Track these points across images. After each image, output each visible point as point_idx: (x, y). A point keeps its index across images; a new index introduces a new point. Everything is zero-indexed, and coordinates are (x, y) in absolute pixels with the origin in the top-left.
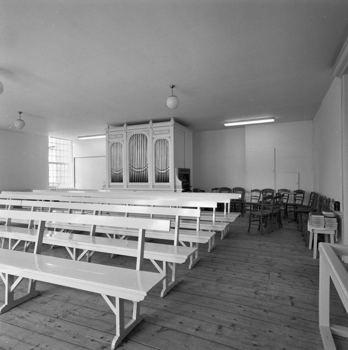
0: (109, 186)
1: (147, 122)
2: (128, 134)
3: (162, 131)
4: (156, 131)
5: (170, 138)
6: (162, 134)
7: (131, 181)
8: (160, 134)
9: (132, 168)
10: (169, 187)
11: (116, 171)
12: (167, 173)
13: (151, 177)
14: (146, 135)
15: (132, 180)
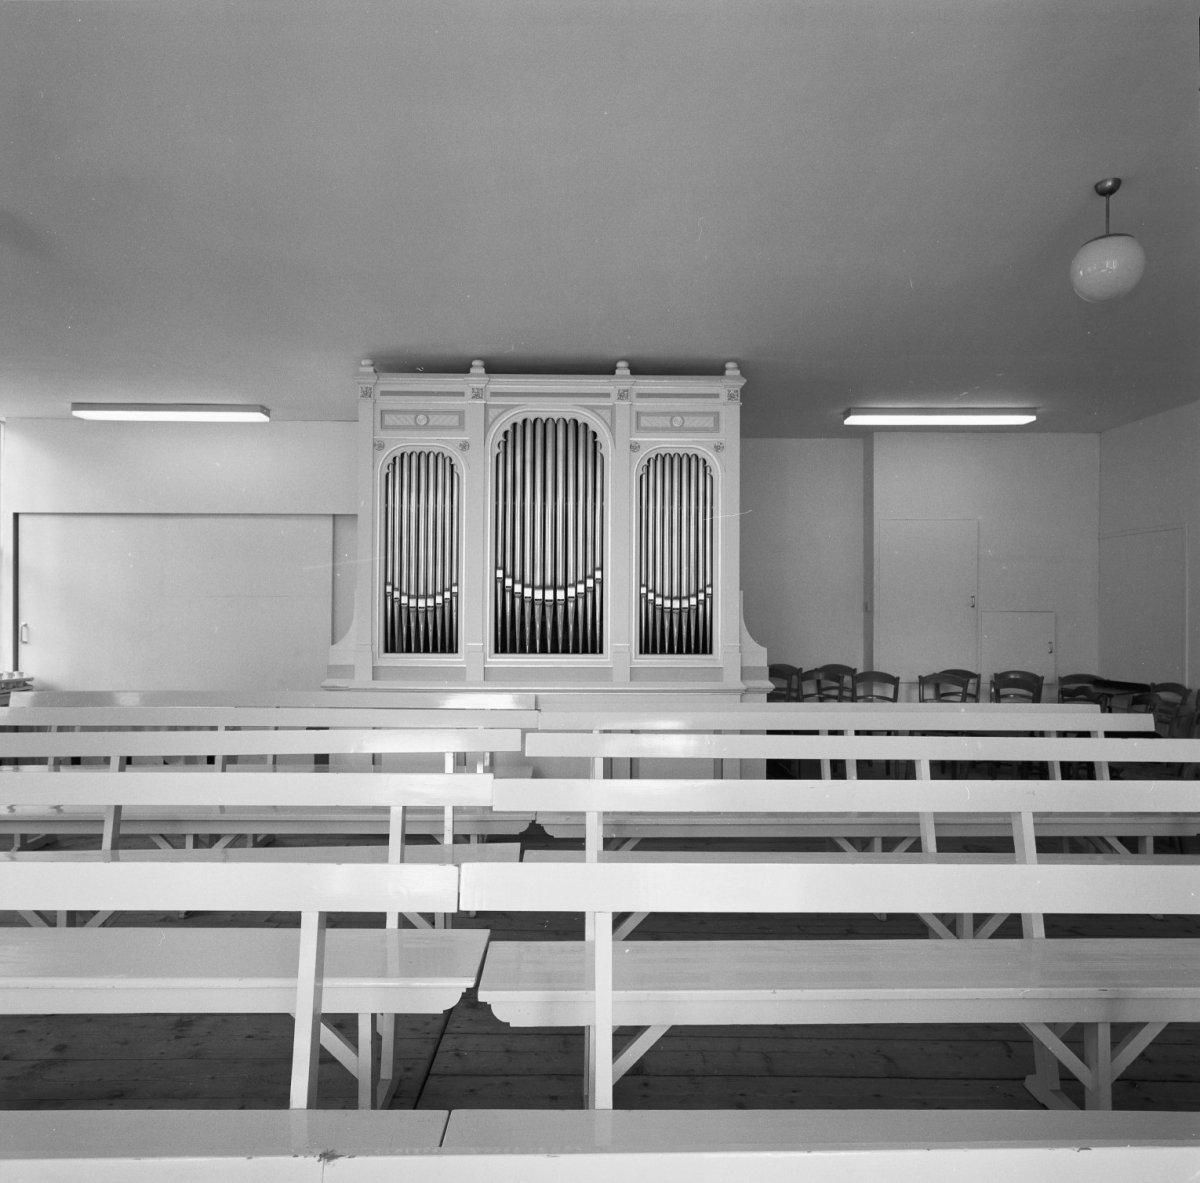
0: (376, 673)
1: (607, 369)
2: (491, 420)
3: (679, 414)
4: (648, 414)
5: (466, 453)
6: (426, 427)
7: (648, 646)
8: (417, 427)
9: (509, 582)
10: (716, 673)
11: (413, 592)
12: (697, 609)
13: (620, 625)
14: (596, 424)
15: (514, 634)
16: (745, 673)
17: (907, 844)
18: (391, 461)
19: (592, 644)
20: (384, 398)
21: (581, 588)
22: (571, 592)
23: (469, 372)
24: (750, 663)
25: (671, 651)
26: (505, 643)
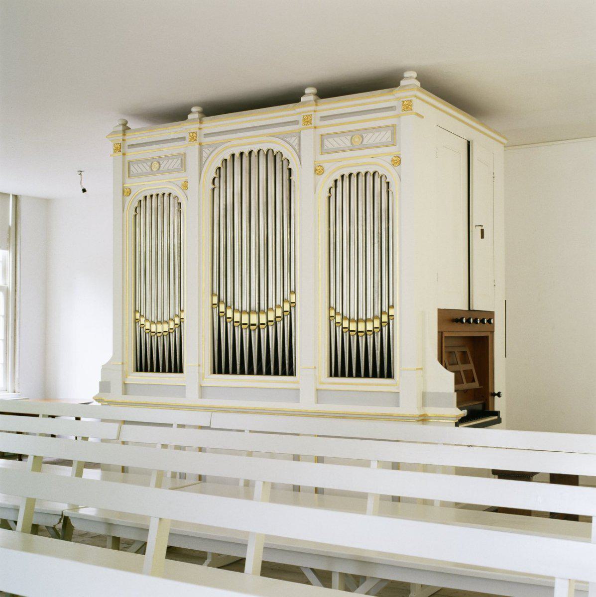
8: (151, 173)
12: (381, 330)
13: (312, 350)
16: (425, 399)
17: (136, 546)
18: (332, 184)
19: (285, 366)
20: (131, 150)
21: (279, 313)
22: (271, 317)
23: (300, 101)
24: (432, 388)
25: (251, 372)
26: (222, 366)
